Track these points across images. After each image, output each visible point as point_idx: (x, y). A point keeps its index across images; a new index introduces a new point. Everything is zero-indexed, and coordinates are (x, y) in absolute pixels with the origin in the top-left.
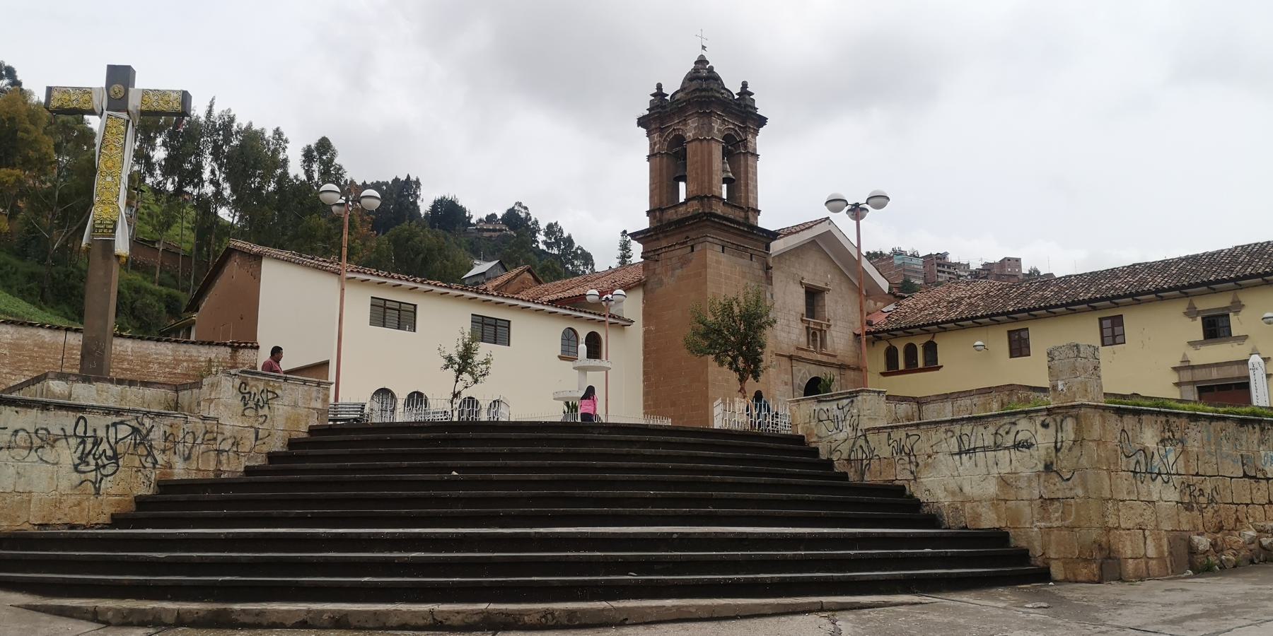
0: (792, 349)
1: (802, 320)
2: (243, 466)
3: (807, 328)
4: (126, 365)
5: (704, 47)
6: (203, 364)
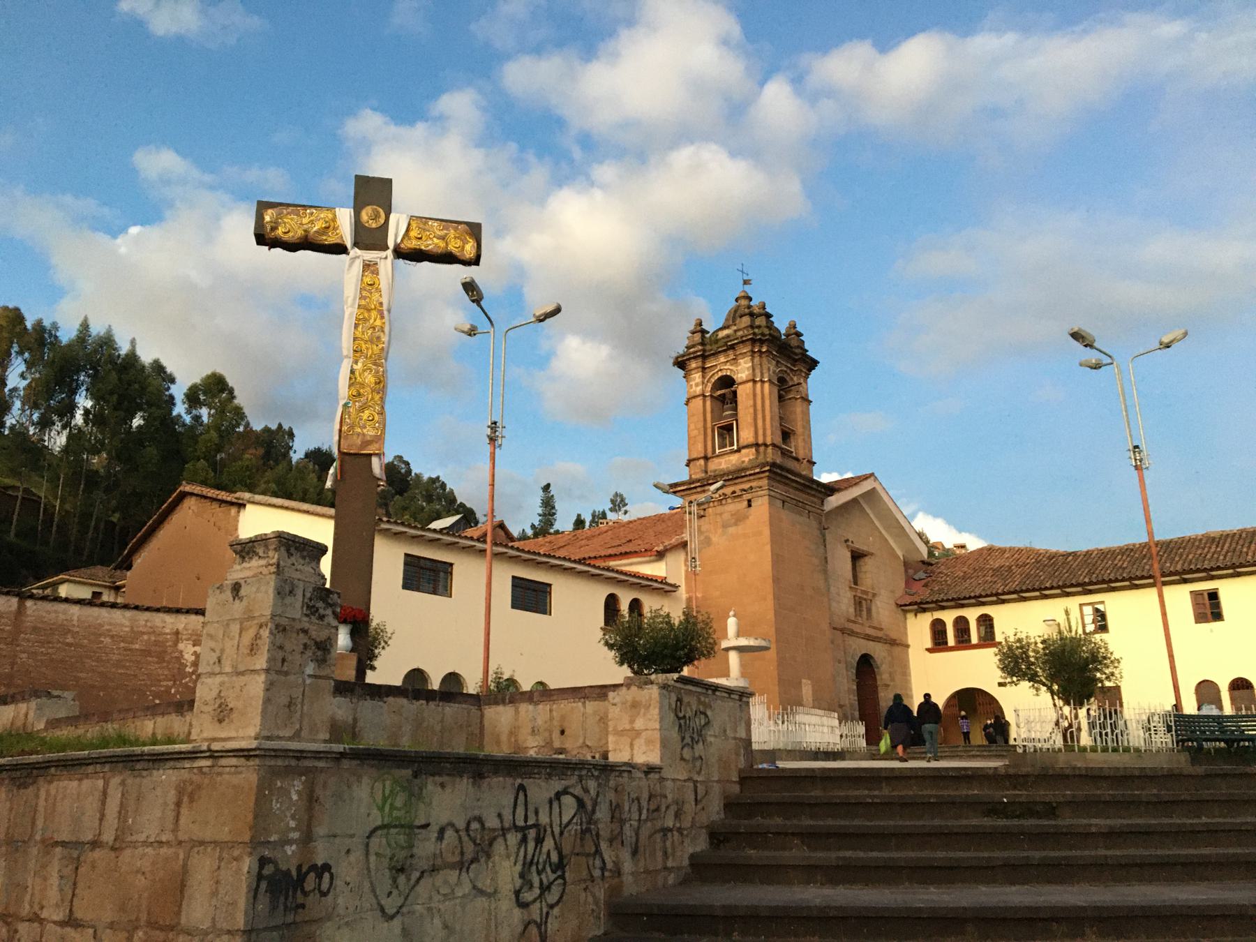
0: (842, 620)
1: (851, 587)
2: (686, 856)
3: (855, 596)
4: (70, 640)
5: (746, 282)
6: (169, 637)
